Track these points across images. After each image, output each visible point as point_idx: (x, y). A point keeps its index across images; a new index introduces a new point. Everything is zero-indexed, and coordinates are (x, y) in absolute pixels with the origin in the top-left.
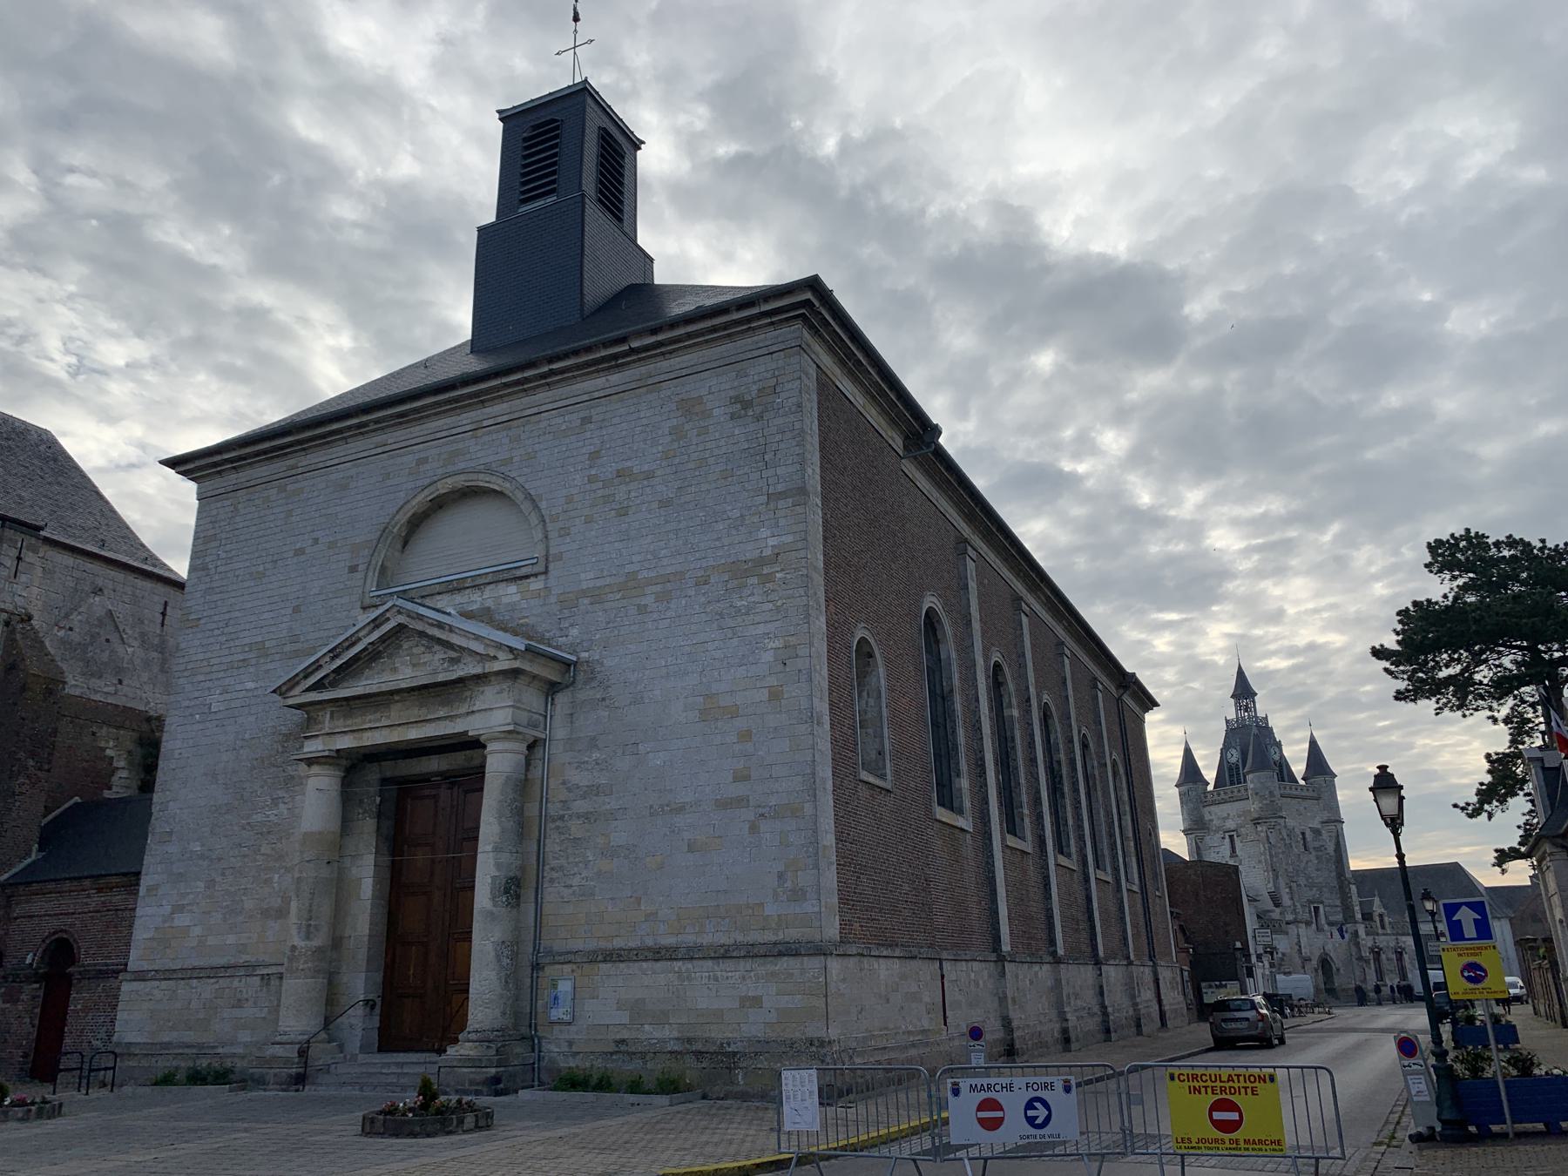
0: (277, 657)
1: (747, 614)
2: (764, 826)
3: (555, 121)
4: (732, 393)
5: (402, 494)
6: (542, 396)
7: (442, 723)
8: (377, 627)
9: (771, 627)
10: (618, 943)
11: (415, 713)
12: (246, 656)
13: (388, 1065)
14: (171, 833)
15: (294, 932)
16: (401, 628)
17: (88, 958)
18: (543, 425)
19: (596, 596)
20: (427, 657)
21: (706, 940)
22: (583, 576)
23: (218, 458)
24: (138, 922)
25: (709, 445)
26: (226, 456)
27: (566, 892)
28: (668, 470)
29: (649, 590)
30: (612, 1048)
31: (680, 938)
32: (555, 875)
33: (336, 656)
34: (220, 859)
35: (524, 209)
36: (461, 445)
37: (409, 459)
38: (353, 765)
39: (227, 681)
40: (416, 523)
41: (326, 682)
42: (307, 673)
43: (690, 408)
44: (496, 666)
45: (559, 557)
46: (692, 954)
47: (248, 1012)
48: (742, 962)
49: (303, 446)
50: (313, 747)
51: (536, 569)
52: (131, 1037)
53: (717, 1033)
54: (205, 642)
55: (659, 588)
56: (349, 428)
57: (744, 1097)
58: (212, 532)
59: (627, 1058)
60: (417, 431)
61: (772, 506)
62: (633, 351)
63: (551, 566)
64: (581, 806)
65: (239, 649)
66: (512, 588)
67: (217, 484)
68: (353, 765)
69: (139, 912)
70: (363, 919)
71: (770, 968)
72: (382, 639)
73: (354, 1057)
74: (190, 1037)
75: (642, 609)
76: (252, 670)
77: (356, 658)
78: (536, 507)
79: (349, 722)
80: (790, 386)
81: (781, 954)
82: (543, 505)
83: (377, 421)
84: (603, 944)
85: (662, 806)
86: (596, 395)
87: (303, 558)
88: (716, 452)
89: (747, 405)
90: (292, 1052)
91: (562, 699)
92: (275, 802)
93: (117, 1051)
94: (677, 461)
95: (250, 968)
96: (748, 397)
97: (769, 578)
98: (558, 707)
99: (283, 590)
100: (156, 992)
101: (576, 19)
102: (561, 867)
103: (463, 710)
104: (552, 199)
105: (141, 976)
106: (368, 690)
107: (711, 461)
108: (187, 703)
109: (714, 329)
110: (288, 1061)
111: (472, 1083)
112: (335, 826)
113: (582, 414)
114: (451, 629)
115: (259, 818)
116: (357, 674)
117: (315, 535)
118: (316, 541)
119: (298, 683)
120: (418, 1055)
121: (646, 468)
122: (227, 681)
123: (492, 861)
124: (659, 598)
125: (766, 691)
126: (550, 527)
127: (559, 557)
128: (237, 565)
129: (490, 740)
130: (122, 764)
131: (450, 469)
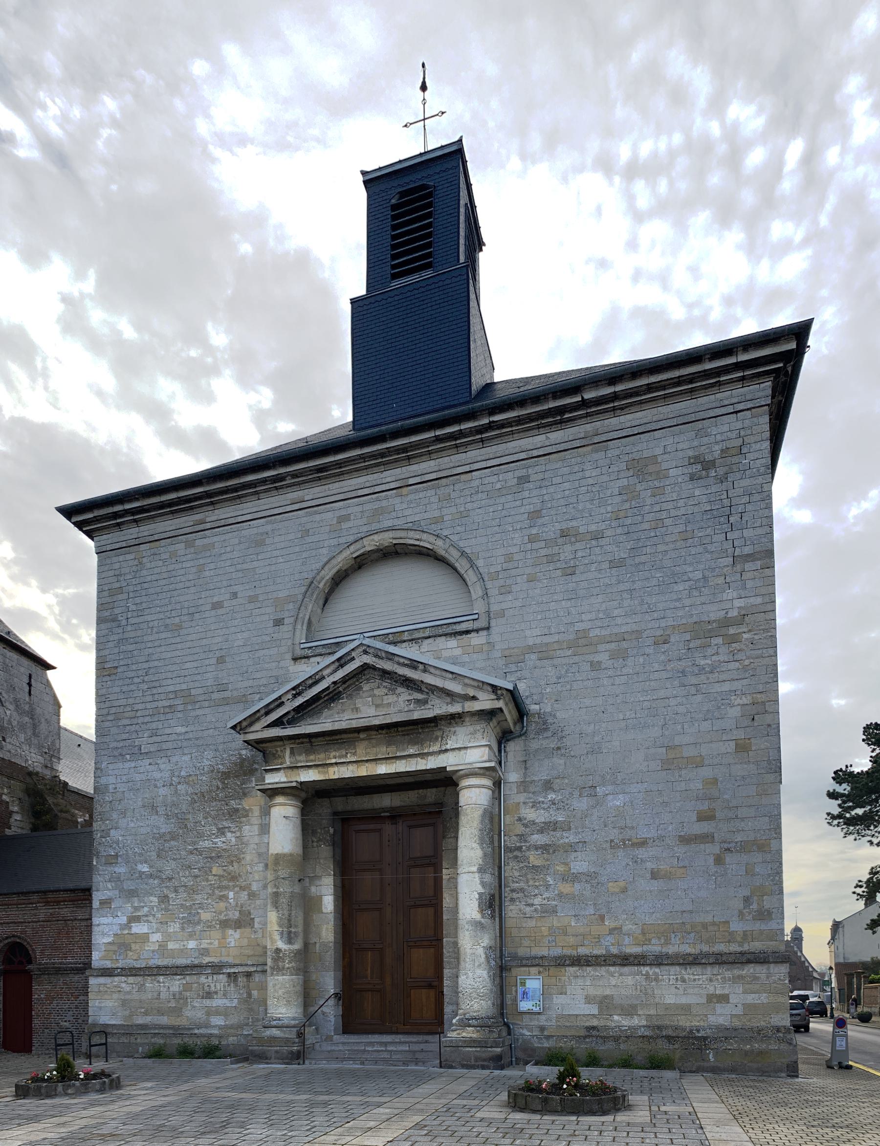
0: (206, 704)
1: (712, 672)
2: (728, 858)
3: (424, 187)
4: (691, 453)
5: (325, 551)
6: (474, 454)
7: (413, 761)
8: (342, 666)
9: (737, 685)
10: (582, 951)
11: (383, 751)
12: (171, 702)
13: (372, 1044)
14: (116, 856)
15: (277, 937)
16: (365, 667)
17: (42, 957)
18: (476, 483)
19: (544, 653)
20: (391, 699)
21: (671, 950)
22: (528, 633)
23: (118, 508)
24: (95, 929)
25: (664, 506)
26: (128, 506)
27: (528, 909)
28: (619, 531)
29: (601, 647)
30: (583, 1033)
31: (645, 948)
32: (515, 895)
33: (299, 694)
34: (170, 879)
35: (396, 284)
36: (384, 503)
37: (328, 516)
38: (310, 797)
39: (154, 726)
40: (340, 579)
41: (285, 720)
42: (268, 710)
43: (641, 468)
44: (476, 706)
45: (502, 614)
46: (660, 961)
47: (218, 1002)
48: (709, 968)
49: (211, 499)
50: (274, 779)
51: (477, 625)
52: (105, 1019)
53: (686, 1022)
54: (125, 689)
55: (613, 646)
56: (264, 481)
57: (714, 1070)
58: (117, 585)
59: (600, 1041)
60: (335, 488)
61: (738, 568)
62: (584, 404)
63: (493, 623)
64: (537, 839)
65: (163, 697)
66: (452, 643)
67: (112, 538)
68: (310, 797)
69: (95, 921)
70: (327, 932)
71: (737, 972)
72: (344, 680)
73: (329, 1038)
74: (164, 1020)
75: (595, 666)
76: (180, 715)
78: (472, 565)
80: (758, 446)
81: (749, 962)
82: (480, 563)
83: (294, 475)
84: (568, 952)
85: (623, 841)
86: (535, 453)
87: (220, 611)
88: (673, 513)
89: (708, 465)
90: (292, 1034)
91: (514, 748)
92: (222, 832)
93: (107, 1031)
94: (629, 521)
95: (216, 968)
96: (709, 457)
97: (735, 639)
98: (511, 756)
99: (204, 642)
100: (123, 985)
101: (424, 88)
102: (522, 890)
103: (435, 748)
104: (428, 274)
105: (107, 972)
106: (337, 726)
107: (668, 522)
108: (114, 744)
109: (679, 381)
110: (287, 1041)
112: (299, 850)
113: (519, 473)
114: (426, 668)
115: (207, 844)
116: (318, 712)
117: (235, 589)
118: (235, 595)
119: (258, 719)
120: (393, 1036)
121: (593, 528)
122: (154, 726)
123: (477, 880)
124: (614, 656)
125: (733, 744)
126: (489, 585)
127: (502, 614)
128: (149, 618)
129: (468, 775)
130: (16, 809)
131: (375, 526)
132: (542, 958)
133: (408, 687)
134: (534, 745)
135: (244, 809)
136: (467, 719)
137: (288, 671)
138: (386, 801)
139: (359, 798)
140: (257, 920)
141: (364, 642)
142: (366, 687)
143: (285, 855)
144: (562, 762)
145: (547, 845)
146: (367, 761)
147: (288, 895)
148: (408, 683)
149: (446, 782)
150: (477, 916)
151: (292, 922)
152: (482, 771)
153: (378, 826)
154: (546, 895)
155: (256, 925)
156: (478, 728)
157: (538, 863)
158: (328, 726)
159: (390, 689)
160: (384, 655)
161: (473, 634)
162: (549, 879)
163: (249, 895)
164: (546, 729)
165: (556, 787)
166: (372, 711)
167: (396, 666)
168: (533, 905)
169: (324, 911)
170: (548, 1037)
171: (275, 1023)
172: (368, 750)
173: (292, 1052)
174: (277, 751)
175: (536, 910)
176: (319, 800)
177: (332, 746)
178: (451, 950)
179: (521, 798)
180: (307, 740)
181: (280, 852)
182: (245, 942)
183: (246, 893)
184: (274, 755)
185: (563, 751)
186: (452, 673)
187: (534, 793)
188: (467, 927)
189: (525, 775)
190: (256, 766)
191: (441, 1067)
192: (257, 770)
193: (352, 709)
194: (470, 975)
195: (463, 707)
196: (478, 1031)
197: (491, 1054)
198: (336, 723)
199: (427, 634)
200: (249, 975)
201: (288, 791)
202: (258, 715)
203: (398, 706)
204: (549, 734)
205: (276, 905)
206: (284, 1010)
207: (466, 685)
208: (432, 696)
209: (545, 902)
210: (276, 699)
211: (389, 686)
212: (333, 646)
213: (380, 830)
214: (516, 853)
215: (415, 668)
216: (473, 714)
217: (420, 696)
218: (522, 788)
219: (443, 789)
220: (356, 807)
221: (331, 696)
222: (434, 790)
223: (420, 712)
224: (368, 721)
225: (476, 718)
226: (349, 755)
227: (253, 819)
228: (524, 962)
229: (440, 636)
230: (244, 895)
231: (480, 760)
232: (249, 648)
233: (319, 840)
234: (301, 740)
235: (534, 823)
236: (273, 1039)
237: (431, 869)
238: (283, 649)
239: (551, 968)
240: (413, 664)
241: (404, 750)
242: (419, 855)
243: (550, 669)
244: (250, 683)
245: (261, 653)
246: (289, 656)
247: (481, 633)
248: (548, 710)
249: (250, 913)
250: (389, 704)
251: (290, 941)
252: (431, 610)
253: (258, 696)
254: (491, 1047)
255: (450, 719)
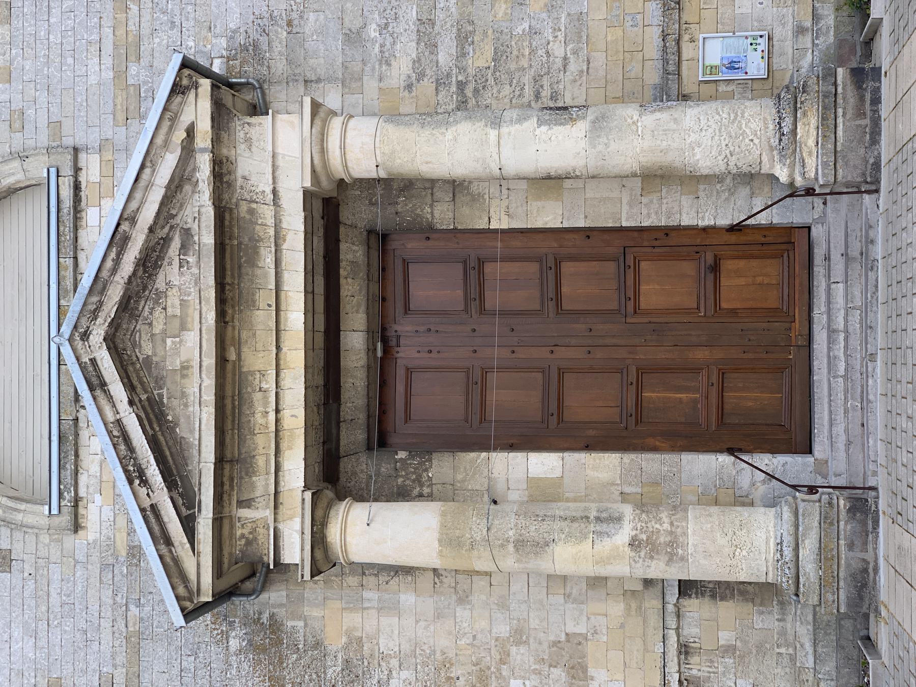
8: (103, 384)
13: (831, 361)
15: (605, 546)
16: (111, 341)
20: (173, 301)
22: (93, 79)
27: (573, 67)
32: (546, 93)
41: (185, 512)
42: (162, 538)
44: (204, 126)
45: (55, 127)
51: (67, 171)
64: (445, 55)
68: (331, 478)
72: (130, 387)
77: (154, 443)
79: (260, 461)
90: (811, 509)
103: (267, 214)
106: (210, 397)
110: (827, 520)
111: (860, 114)
114: (127, 218)
116: (180, 445)
119: (176, 561)
127: (55, 127)
132: (664, 37)
133: (157, 266)
134: (280, 66)
135: (346, 648)
136: (225, 151)
137: (95, 541)
138: (355, 341)
139: (345, 396)
140: (571, 628)
141: (67, 336)
142: (147, 349)
143: (443, 526)
144: (312, 16)
145: (458, 36)
146: (278, 347)
147: (522, 521)
148: (150, 262)
149: (328, 207)
150: (581, 128)
151: (578, 515)
152: (318, 122)
153: (401, 373)
154: (548, 34)
155: (581, 629)
156: (242, 134)
157: (489, 52)
158: (208, 416)
159: (157, 302)
160: (95, 299)
161: (82, 178)
162: (519, 30)
163: (518, 643)
164: (256, 45)
165: (358, 23)
166: (191, 338)
167: (117, 278)
168: (565, 58)
169: (558, 473)
170: (816, 17)
171: (788, 553)
172: (259, 346)
173: (852, 511)
174: (243, 536)
175: (575, 52)
176: (343, 479)
177: (244, 419)
178: (645, 211)
179: (371, 85)
180: (227, 467)
181: (436, 535)
182: (616, 657)
183: (514, 650)
184: (249, 543)
185: (295, 15)
186: (143, 167)
187: (364, 62)
188: (600, 147)
189: (331, 80)
190: (265, 618)
191: (877, 191)
192: (272, 616)
193: (184, 376)
194: (693, 137)
195: (203, 150)
196: (805, 114)
197: (850, 89)
198: (205, 397)
199: (69, 262)
200: (685, 650)
201: (319, 513)
202: (168, 559)
203: (189, 284)
204: (264, 40)
205: (541, 546)
206: (762, 535)
207: (166, 143)
208: (177, 220)
209: (561, 36)
210: (145, 518)
211: (150, 304)
212: (64, 449)
213: (409, 371)
214: (469, 92)
215: (126, 239)
216: (216, 140)
217: (176, 244)
218: (354, 85)
219: (342, 229)
220: (361, 402)
221: (154, 416)
222: (343, 246)
223: (204, 232)
224: (208, 372)
225: (224, 135)
226: (264, 386)
227: (367, 628)
228: (671, 68)
229: (76, 239)
230: (518, 654)
231: (298, 129)
232: (43, 626)
233: (419, 481)
234: (225, 479)
235: (417, 61)
236: (824, 555)
237: (488, 268)
238: (55, 554)
239: (685, 18)
240: (118, 241)
241: (266, 275)
242: (460, 293)
243: (157, 40)
244: (106, 624)
245: (55, 599)
246: (70, 540)
247: (82, 163)
248: (223, 42)
249: (556, 643)
250: (183, 304)
251: (617, 519)
252: (30, 271)
253: (132, 607)
254: (835, 84)
255: (221, 181)
